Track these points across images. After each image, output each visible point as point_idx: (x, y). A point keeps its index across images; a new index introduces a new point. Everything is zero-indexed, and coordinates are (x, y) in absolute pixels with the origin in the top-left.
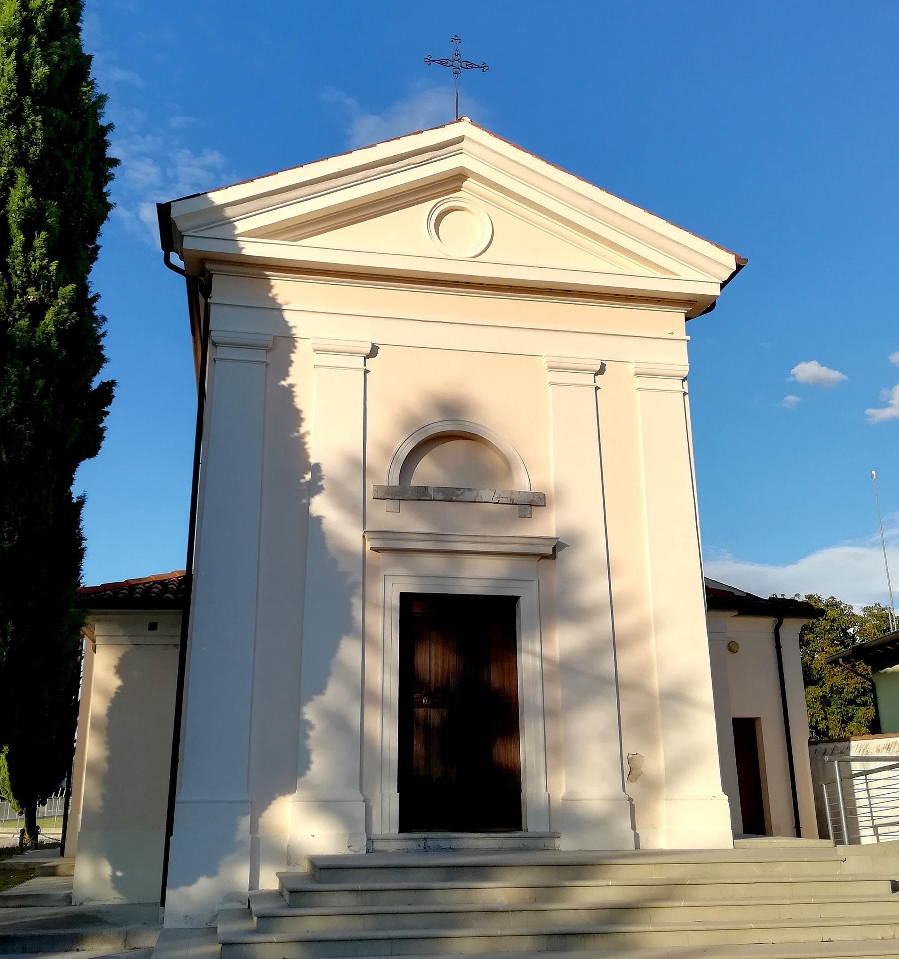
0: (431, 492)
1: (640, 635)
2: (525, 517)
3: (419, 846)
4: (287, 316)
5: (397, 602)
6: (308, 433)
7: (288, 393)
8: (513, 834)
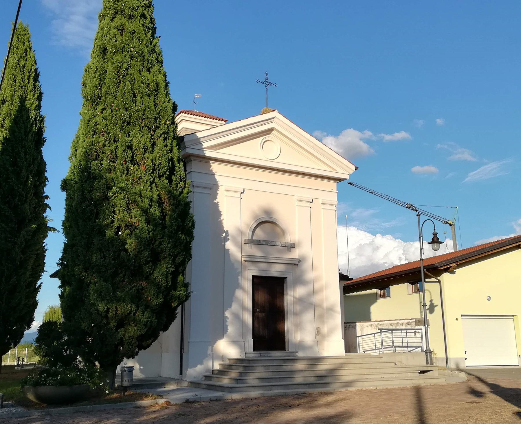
0: (261, 242)
1: (321, 290)
4: (216, 177)
6: (223, 219)
7: (217, 205)
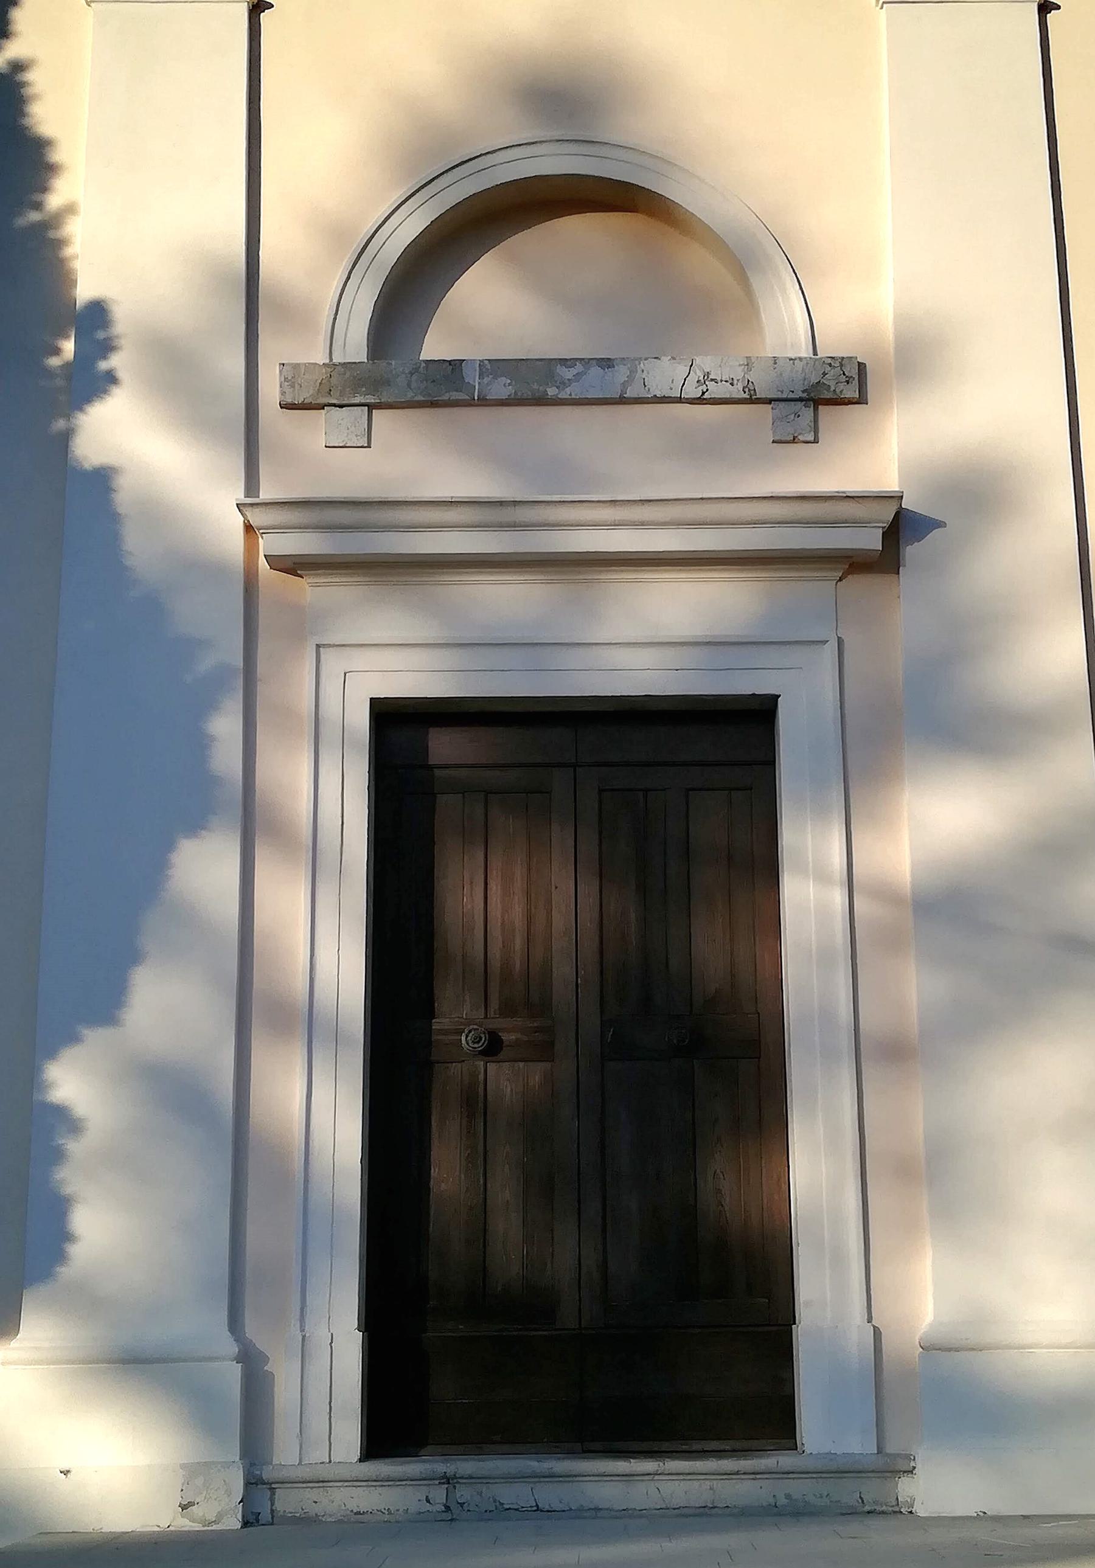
0: (472, 377)
2: (794, 440)
3: (428, 1501)
5: (361, 720)
6: (70, 209)
8: (750, 1462)
